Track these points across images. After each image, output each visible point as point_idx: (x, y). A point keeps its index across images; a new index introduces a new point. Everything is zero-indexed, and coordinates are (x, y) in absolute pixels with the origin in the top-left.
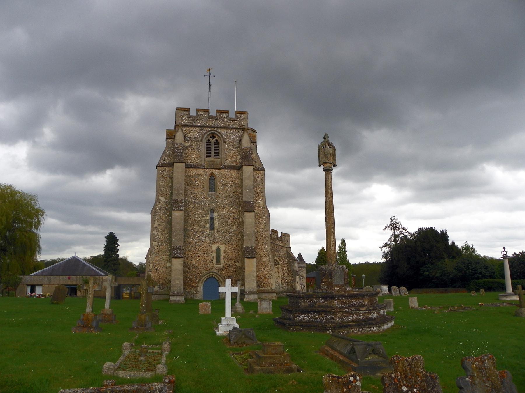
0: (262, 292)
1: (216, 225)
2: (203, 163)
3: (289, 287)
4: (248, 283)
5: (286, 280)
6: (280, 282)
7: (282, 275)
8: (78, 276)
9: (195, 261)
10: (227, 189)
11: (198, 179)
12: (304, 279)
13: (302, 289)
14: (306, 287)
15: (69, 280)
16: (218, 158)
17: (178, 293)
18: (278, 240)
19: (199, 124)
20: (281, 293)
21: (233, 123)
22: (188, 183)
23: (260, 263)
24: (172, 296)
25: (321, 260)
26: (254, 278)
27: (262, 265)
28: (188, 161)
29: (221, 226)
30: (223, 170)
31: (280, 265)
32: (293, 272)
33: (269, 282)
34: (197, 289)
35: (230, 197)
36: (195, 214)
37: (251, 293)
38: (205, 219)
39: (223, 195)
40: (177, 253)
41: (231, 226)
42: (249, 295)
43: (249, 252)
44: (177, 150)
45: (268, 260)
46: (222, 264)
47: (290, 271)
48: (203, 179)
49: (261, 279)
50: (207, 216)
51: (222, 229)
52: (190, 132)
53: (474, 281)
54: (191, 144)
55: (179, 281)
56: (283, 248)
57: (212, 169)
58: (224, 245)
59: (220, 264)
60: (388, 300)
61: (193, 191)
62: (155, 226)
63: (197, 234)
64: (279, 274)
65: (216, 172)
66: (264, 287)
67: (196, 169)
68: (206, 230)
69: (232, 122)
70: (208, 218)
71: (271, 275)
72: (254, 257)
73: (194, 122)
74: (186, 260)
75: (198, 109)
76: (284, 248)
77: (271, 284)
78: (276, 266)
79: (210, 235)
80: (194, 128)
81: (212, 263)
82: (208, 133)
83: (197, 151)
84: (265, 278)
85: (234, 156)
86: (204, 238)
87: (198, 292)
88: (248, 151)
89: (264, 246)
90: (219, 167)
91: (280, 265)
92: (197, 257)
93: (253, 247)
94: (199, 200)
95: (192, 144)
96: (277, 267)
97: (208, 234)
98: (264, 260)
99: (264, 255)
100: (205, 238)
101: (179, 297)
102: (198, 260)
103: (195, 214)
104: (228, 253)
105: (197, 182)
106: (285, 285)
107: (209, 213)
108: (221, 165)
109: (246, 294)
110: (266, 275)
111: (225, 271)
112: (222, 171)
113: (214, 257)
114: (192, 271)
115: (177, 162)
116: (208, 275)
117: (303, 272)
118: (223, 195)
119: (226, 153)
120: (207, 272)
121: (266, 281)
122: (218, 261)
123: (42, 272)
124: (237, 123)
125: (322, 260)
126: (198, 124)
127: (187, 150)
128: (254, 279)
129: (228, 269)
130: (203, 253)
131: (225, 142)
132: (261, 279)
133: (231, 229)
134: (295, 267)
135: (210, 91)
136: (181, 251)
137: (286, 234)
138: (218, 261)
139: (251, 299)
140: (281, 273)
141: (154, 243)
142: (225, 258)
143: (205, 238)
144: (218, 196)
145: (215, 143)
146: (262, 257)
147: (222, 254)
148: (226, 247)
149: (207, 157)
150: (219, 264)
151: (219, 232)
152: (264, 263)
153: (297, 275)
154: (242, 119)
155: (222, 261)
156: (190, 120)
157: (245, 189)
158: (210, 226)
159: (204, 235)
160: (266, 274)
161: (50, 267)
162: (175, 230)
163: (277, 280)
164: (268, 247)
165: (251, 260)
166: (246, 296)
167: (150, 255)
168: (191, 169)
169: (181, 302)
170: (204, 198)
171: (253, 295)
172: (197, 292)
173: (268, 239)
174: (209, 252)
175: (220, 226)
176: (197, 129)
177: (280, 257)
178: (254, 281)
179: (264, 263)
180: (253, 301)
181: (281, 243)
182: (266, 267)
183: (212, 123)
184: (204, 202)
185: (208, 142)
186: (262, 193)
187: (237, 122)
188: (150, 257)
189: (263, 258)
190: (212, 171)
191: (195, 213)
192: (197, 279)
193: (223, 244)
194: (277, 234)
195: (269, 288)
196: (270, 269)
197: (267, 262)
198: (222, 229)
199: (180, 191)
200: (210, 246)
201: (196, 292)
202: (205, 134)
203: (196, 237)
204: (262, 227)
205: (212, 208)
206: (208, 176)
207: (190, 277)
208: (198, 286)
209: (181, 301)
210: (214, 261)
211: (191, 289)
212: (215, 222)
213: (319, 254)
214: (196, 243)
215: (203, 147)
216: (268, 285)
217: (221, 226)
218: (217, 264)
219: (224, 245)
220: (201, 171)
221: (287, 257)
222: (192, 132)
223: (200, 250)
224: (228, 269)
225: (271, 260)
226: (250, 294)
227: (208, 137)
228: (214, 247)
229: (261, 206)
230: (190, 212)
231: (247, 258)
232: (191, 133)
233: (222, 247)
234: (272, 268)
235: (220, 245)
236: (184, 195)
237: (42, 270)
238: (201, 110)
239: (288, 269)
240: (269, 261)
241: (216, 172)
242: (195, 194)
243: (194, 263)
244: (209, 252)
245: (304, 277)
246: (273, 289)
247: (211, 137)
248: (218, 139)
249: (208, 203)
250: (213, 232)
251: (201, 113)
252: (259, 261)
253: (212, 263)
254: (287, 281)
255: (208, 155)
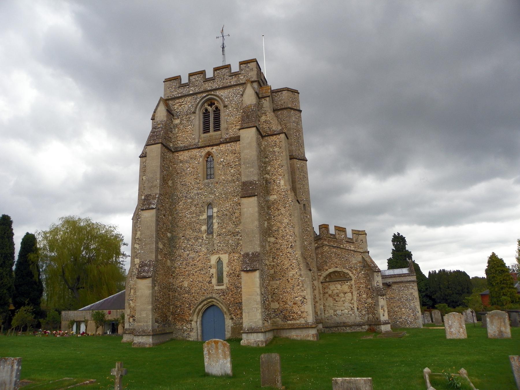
0: (290, 327)
1: (216, 226)
2: (197, 141)
3: (370, 315)
4: (247, 314)
5: (366, 303)
6: (356, 309)
7: (358, 297)
8: (118, 309)
9: (187, 282)
10: (230, 171)
11: (190, 164)
12: (415, 300)
13: (414, 316)
14: (420, 312)
15: (110, 315)
16: (219, 130)
17: (144, 331)
18: (347, 241)
19: (192, 92)
20: (358, 325)
21: (236, 79)
22: (178, 172)
23: (284, 279)
24: (137, 336)
25: (492, 270)
26: (257, 305)
27: (289, 282)
28: (178, 143)
29: (222, 227)
30: (224, 145)
31: (353, 281)
32: (374, 291)
33: (302, 310)
34: (191, 324)
35: (234, 182)
36: (187, 214)
37: (252, 331)
38: (200, 218)
39: (224, 180)
40: (144, 271)
41: (237, 224)
42: (248, 334)
43: (248, 262)
44: (155, 129)
45: (298, 274)
46: (225, 285)
47: (369, 289)
48: (197, 162)
49: (288, 306)
50: (203, 215)
51: (224, 230)
52: (181, 105)
53: (329, 243)
54: (182, 120)
55: (146, 313)
56: (356, 253)
57: (209, 146)
58: (227, 255)
59: (223, 285)
60: (349, 382)
61: (184, 181)
62: (137, 237)
63: (190, 243)
64: (352, 295)
65: (214, 150)
66: (293, 319)
67: (187, 151)
68: (201, 235)
69: (235, 77)
70: (205, 216)
71: (305, 298)
72: (255, 268)
73: (185, 91)
74: (176, 281)
75: (191, 73)
76: (358, 253)
77: (305, 315)
78: (347, 282)
79: (207, 242)
80: (186, 99)
81: (211, 283)
82: (203, 100)
83: (189, 127)
84: (295, 304)
85: (239, 123)
86: (199, 246)
87: (193, 329)
88: (251, 109)
89: (290, 250)
90: (217, 142)
91: (353, 281)
92: (191, 276)
93: (257, 252)
94: (192, 193)
95: (183, 120)
96: (348, 284)
97: (205, 241)
98: (291, 274)
99: (291, 265)
100: (201, 246)
101: (145, 337)
102: (191, 280)
103: (187, 214)
104: (234, 267)
105: (189, 169)
106: (364, 313)
107: (205, 210)
108: (221, 138)
109: (243, 333)
110: (297, 299)
111: (230, 295)
112: (223, 147)
113: (213, 274)
114: (183, 298)
115: (151, 144)
116: (205, 302)
117: (413, 288)
118: (224, 180)
119: (228, 120)
120: (204, 297)
121: (296, 309)
122: (220, 281)
123: (91, 307)
124: (242, 77)
125: (492, 270)
126: (191, 92)
127: (177, 129)
128: (257, 306)
129: (234, 292)
130: (198, 269)
131: (225, 106)
132: (288, 306)
133: (237, 230)
134: (375, 282)
135: (223, 54)
136: (150, 267)
137: (359, 231)
138: (220, 281)
139: (253, 341)
140: (355, 293)
141: (136, 260)
142: (229, 275)
143: (200, 247)
144: (217, 183)
145: (214, 111)
146: (288, 269)
147: (226, 269)
148: (230, 257)
149: (204, 133)
150: (221, 285)
151: (220, 235)
152: (292, 279)
153: (381, 295)
154: (248, 69)
155: (226, 280)
156: (181, 90)
157: (244, 164)
158: (208, 229)
159: (198, 243)
160: (296, 297)
161: (102, 300)
162: (145, 238)
163: (350, 304)
164: (296, 252)
165: (250, 274)
166: (244, 336)
167: (131, 277)
168: (182, 153)
169: (147, 346)
170: (199, 189)
171: (255, 334)
172: (191, 330)
173: (296, 238)
174: (206, 267)
175: (221, 227)
176: (189, 99)
177: (351, 268)
178: (257, 311)
179: (292, 279)
180: (255, 345)
181: (352, 246)
182: (295, 285)
183: (208, 86)
184: (198, 194)
185: (206, 114)
186: (282, 168)
187: (241, 76)
188: (131, 280)
189: (290, 271)
190: (209, 149)
191: (187, 212)
192: (190, 310)
193: (225, 253)
194: (344, 233)
195: (302, 321)
196: (303, 288)
197: (297, 276)
198: (224, 230)
199: (155, 183)
200: (207, 257)
201: (189, 330)
202: (198, 103)
203: (188, 246)
204: (286, 221)
205: (210, 202)
206: (203, 157)
207: (181, 306)
208: (191, 321)
209: (147, 344)
210: (214, 281)
211: (182, 325)
212: (214, 221)
213: (489, 262)
214: (188, 255)
215: (197, 120)
216: (300, 315)
217: (222, 227)
218: (218, 285)
219: (227, 255)
220: (195, 152)
221: (364, 267)
222: (183, 105)
223: (195, 265)
224: (234, 292)
225: (302, 273)
226: (251, 333)
227: (205, 106)
228: (214, 259)
229: (282, 187)
230: (180, 212)
231: (244, 271)
232: (182, 106)
233: (225, 258)
234: (305, 286)
235: (221, 256)
236: (159, 188)
237: (92, 304)
238: (195, 74)
239: (366, 287)
240: (301, 275)
241: (214, 150)
242: (186, 185)
243: (186, 286)
244: (206, 267)
245: (415, 296)
246: (309, 321)
247: (209, 105)
248: (218, 105)
249: (204, 195)
250: (211, 236)
251: (194, 77)
252: (283, 276)
253: (210, 285)
254: (366, 305)
255: (206, 130)
